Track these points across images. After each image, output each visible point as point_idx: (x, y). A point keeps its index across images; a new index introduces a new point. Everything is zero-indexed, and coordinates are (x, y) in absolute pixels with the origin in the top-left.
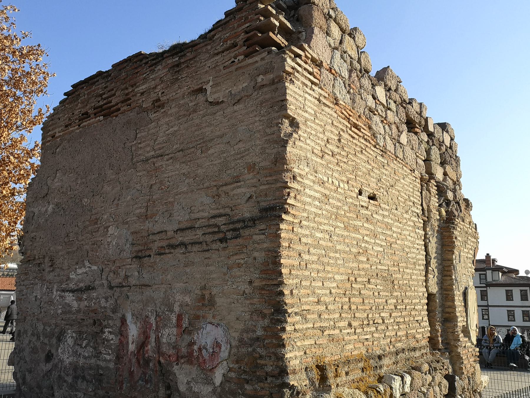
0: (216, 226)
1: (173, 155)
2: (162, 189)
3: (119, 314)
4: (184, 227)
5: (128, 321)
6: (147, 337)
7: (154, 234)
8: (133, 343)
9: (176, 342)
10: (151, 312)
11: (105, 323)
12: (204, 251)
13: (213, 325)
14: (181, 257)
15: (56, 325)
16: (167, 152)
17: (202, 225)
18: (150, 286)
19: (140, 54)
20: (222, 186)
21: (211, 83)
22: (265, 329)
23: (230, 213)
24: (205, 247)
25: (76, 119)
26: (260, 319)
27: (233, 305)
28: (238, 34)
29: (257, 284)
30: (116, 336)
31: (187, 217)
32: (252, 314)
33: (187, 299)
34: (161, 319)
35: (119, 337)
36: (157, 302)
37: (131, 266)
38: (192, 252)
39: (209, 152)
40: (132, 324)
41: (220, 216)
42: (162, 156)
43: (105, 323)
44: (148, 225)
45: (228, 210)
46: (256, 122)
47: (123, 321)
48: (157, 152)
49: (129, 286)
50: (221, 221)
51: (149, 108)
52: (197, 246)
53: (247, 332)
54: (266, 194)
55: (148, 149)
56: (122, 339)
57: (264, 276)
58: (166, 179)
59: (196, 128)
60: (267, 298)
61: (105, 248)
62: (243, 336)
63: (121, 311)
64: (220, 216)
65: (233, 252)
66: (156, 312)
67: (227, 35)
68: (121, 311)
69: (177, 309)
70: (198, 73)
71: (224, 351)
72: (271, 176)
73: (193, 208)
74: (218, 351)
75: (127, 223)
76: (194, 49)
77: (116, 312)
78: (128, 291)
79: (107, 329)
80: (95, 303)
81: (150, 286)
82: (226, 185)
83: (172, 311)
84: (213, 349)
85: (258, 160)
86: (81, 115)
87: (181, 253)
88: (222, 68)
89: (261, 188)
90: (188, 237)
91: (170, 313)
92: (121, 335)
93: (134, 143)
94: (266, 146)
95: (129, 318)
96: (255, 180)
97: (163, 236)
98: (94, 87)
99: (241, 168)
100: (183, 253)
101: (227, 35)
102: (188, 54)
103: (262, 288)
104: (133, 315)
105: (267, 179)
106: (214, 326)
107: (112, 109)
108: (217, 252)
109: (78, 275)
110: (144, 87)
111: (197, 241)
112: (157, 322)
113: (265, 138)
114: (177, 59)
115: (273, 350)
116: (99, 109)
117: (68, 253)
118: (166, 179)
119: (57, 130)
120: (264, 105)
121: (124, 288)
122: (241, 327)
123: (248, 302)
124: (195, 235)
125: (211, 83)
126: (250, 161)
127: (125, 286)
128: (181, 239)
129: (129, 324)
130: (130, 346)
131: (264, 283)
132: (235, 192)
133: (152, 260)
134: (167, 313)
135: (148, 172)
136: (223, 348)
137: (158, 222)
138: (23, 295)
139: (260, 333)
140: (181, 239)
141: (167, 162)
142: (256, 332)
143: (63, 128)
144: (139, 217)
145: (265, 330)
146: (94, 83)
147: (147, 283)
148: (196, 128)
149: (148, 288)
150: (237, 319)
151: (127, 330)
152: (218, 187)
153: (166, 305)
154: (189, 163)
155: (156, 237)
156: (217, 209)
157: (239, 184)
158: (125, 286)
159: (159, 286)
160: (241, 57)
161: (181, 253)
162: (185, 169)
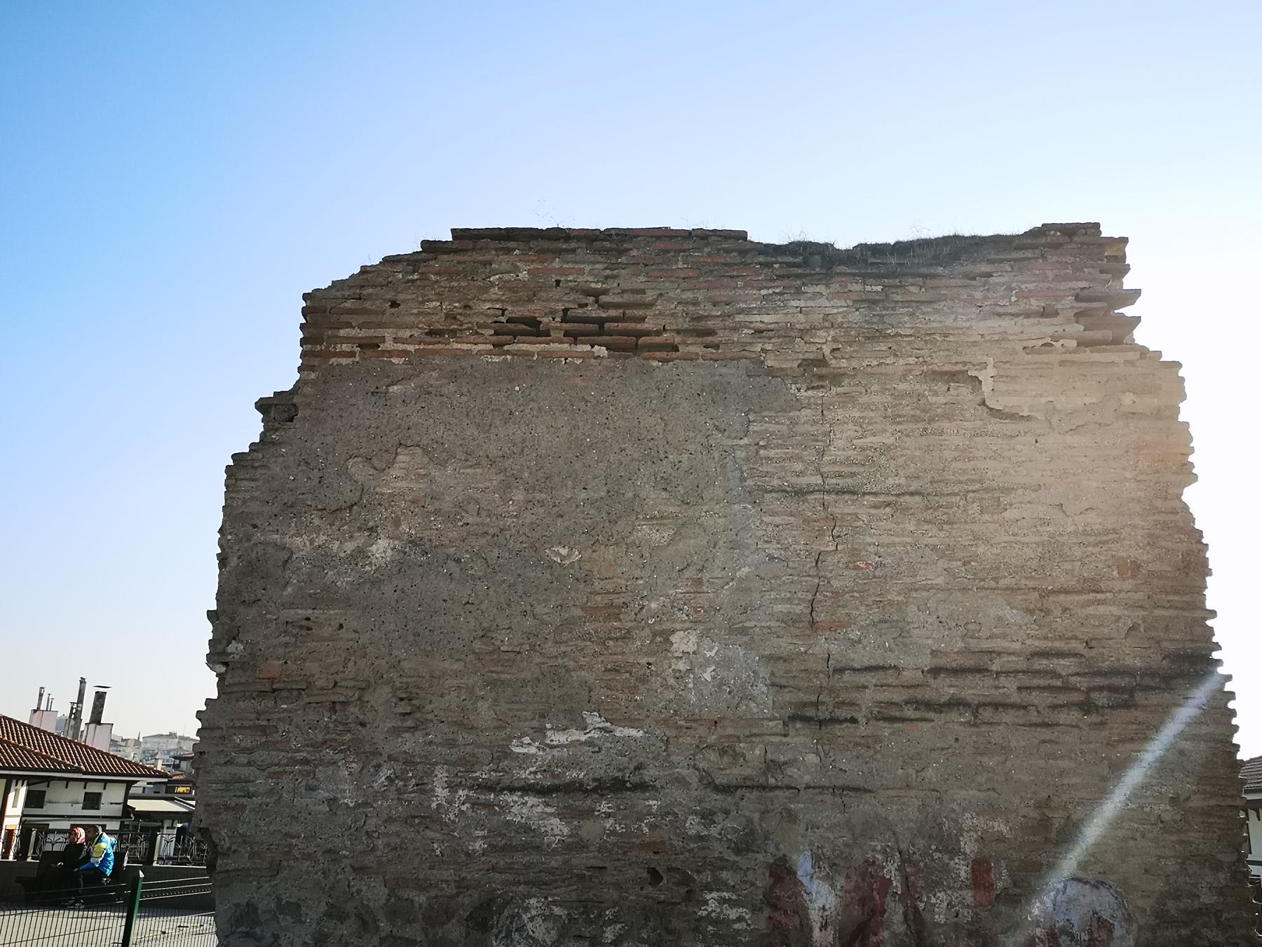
0: (1054, 674)
1: (893, 498)
2: (857, 568)
3: (760, 857)
4: (954, 665)
5: (800, 873)
6: (873, 911)
7: (854, 670)
8: (824, 927)
9: (977, 919)
10: (884, 852)
11: (706, 877)
12: (1031, 725)
13: (1086, 883)
14: (963, 732)
15: (462, 885)
16: (868, 488)
17: (1013, 666)
18: (870, 791)
19: (742, 235)
20: (1053, 592)
21: (991, 371)
22: (1221, 892)
23: (1085, 652)
24: (1033, 717)
25: (486, 326)
26: (1207, 871)
27: (1131, 843)
28: (1059, 293)
29: (1196, 802)
30: (755, 909)
31: (960, 645)
32: (1184, 863)
33: (999, 826)
34: (919, 870)
35: (767, 912)
36: (898, 829)
37: (784, 739)
38: (999, 724)
39: (1006, 514)
40: (816, 882)
41: (1060, 654)
42: (854, 493)
43: (706, 877)
44: (822, 645)
45: (1079, 647)
46: (1126, 480)
47: (782, 871)
48: (829, 481)
49: (789, 787)
50: (1064, 665)
51: (789, 372)
52: (1012, 712)
53: (1177, 898)
54: (1167, 626)
55: (798, 467)
56: (779, 916)
57: (1208, 788)
58: (872, 549)
59: (956, 454)
60: (1219, 832)
61: (666, 686)
62: (1165, 905)
63: (772, 848)
64: (1060, 654)
65: (1119, 734)
66: (900, 853)
67: (1030, 286)
68: (772, 848)
69: (969, 845)
70: (951, 338)
71: (1122, 938)
72: (1176, 593)
73: (971, 627)
74: (1105, 937)
75: (744, 631)
76: (930, 283)
77: (748, 850)
78: (791, 800)
79: (715, 895)
80: (652, 827)
81: (870, 791)
82: (1066, 592)
83: (955, 852)
84: (1091, 933)
85: (1145, 558)
86: (503, 319)
87: (962, 724)
88: (1019, 347)
89: (1157, 612)
90: (974, 688)
91: (946, 857)
92: (774, 907)
93: (742, 442)
94: (1158, 532)
95: (803, 865)
96: (1140, 596)
97: (890, 678)
98: (557, 264)
99: (1100, 565)
100: (969, 723)
101: (1030, 286)
102: (912, 289)
103: (1207, 813)
104: (817, 859)
105: (1170, 598)
106: (1087, 887)
107: (642, 340)
108: (1076, 731)
109: (552, 747)
110: (767, 319)
111: (1001, 700)
112: (906, 878)
113: (1155, 518)
114: (879, 288)
115: (1242, 931)
116: (590, 327)
117: (492, 684)
118: (872, 549)
119: (388, 334)
120: (1144, 451)
121: (777, 792)
122: (1157, 888)
123: (1174, 838)
124: (997, 687)
125: (991, 371)
126: (1124, 555)
127: (777, 787)
128: (952, 691)
129: (805, 880)
130: (817, 933)
131: (1213, 802)
132: (1091, 610)
133: (863, 730)
134: (937, 855)
135: (804, 521)
136: (1118, 932)
137: (865, 642)
138: (249, 796)
139: (1207, 898)
140: (952, 691)
141: (873, 511)
142: (1199, 897)
143: (416, 333)
144: (790, 621)
145: (1221, 894)
146: (558, 253)
147: (861, 783)
148: (956, 454)
149: (867, 796)
150: (1146, 871)
151: (797, 895)
152: (1045, 594)
153: (930, 837)
154: (946, 527)
155: (869, 679)
156: (1046, 638)
157: (1099, 596)
158: (777, 787)
159: (902, 793)
160: (1073, 344)
161: (962, 724)
162: (935, 537)
